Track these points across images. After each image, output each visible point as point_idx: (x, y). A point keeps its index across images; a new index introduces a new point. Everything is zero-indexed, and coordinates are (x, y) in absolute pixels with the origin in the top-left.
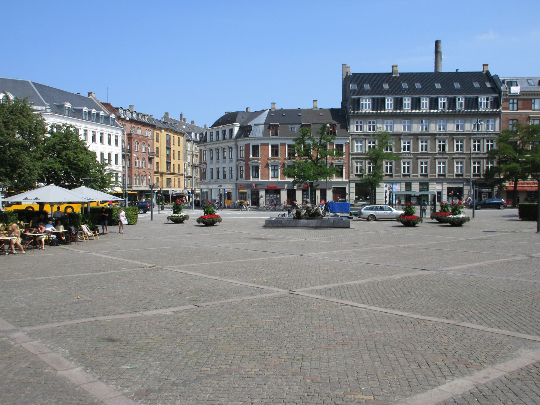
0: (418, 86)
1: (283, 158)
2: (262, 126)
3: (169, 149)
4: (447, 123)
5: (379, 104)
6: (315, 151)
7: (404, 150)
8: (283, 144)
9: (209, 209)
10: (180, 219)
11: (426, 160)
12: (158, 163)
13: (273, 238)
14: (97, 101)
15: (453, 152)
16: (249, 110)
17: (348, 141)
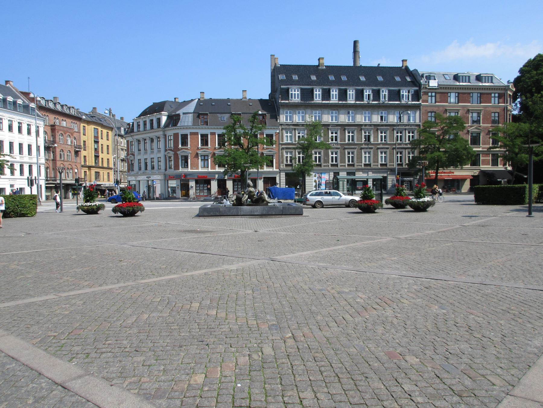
0: (344, 78)
1: (213, 148)
2: (191, 115)
3: (96, 142)
4: (372, 114)
5: (307, 95)
6: (246, 139)
7: (332, 140)
8: (213, 134)
9: (127, 196)
10: (94, 209)
11: (353, 150)
12: (85, 157)
13: (211, 230)
14: (15, 89)
15: (377, 143)
16: (177, 100)
17: (278, 131)
